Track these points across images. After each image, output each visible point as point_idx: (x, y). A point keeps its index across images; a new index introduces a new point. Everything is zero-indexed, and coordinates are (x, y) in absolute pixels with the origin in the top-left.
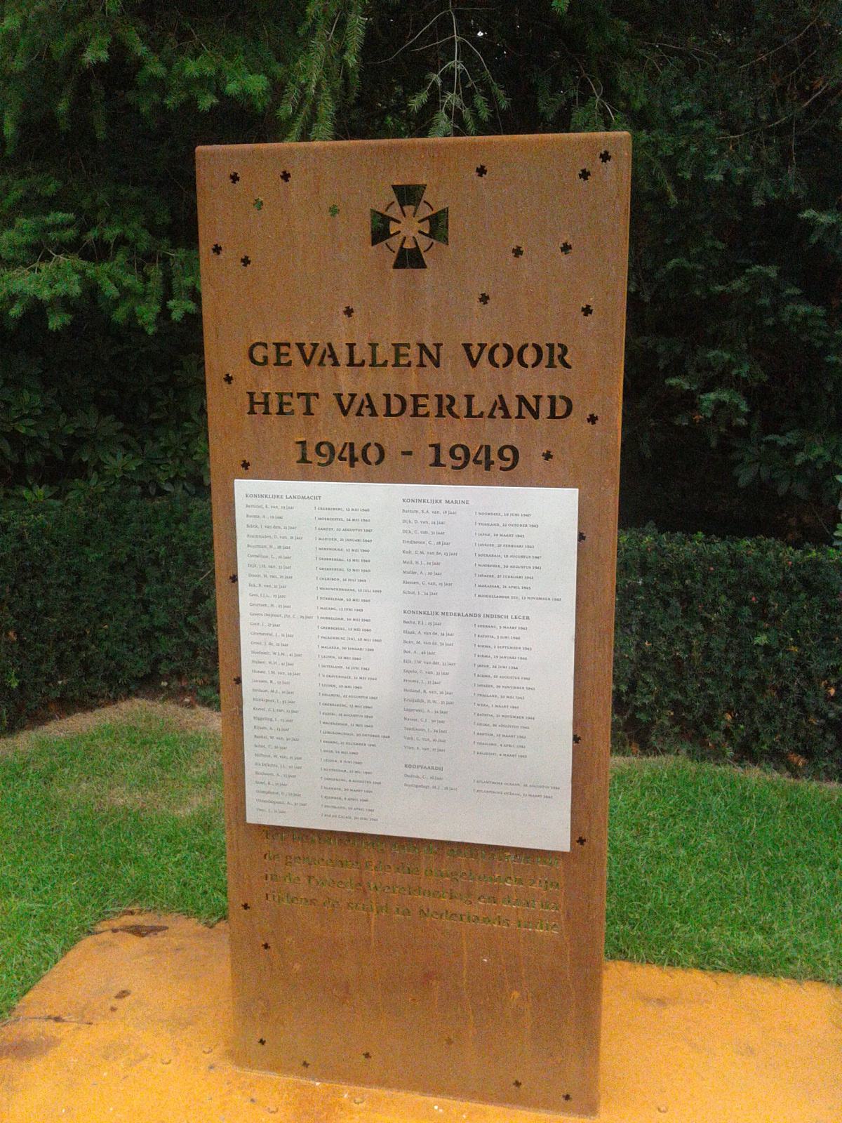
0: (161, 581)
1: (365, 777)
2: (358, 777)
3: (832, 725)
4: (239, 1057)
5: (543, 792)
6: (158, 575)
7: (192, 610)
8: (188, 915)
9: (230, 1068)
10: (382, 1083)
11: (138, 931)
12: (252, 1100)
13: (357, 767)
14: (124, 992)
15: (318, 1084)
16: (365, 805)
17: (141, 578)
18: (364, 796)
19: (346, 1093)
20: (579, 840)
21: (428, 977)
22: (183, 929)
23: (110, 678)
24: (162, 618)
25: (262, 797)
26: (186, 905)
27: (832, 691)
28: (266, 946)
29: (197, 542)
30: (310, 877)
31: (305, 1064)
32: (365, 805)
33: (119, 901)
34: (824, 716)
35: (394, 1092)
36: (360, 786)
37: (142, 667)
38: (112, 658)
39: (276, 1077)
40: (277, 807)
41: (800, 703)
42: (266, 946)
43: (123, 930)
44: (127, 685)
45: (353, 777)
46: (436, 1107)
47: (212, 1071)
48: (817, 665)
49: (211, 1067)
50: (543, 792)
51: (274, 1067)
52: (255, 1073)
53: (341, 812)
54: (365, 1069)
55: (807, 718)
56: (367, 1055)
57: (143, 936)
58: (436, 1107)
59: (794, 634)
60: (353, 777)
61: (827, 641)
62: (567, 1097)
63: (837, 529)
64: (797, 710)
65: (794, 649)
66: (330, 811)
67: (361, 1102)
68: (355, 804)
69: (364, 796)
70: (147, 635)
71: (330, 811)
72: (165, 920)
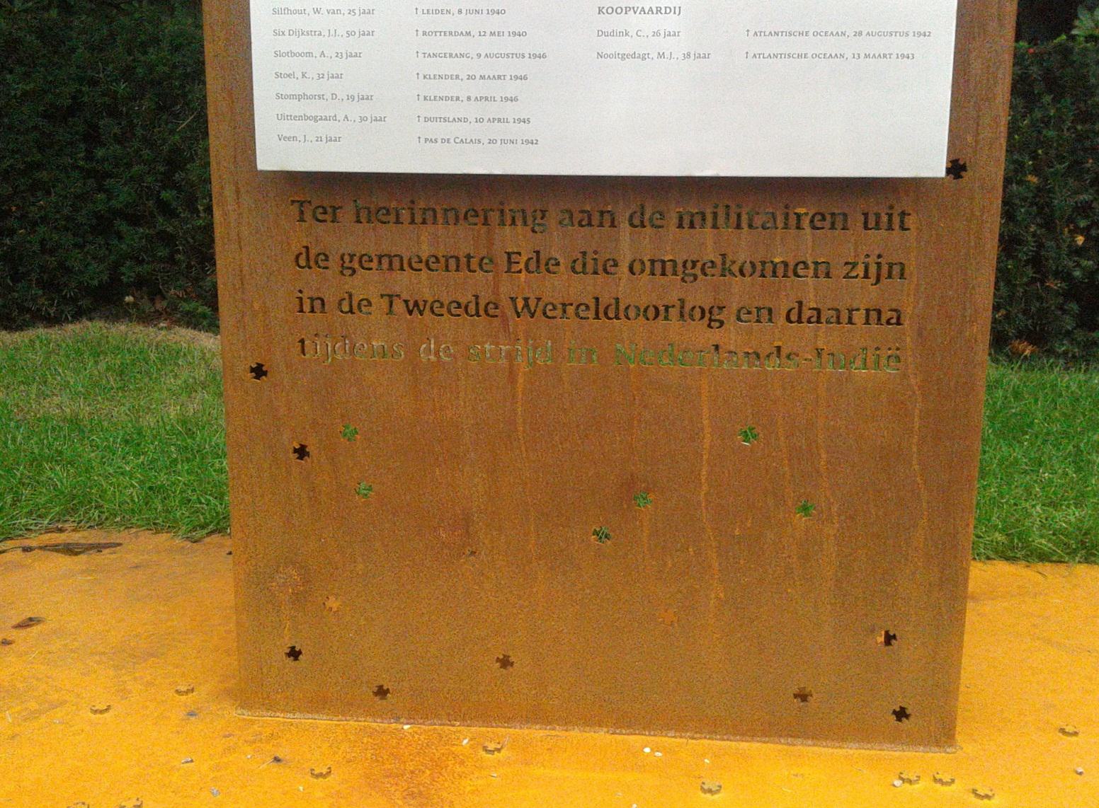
0: (119, 140)
1: (512, 45)
2: (497, 45)
3: (1073, 292)
4: (251, 691)
5: (899, 45)
6: (116, 130)
7: (167, 181)
8: (155, 527)
9: (233, 714)
10: (537, 715)
11: (70, 550)
12: (277, 760)
13: (495, 23)
14: (31, 619)
15: (406, 727)
16: (510, 111)
17: (92, 137)
18: (511, 88)
19: (465, 737)
20: (956, 168)
21: (630, 490)
22: (143, 546)
23: (51, 286)
24: (124, 195)
25: (292, 107)
26: (155, 511)
27: (1080, 240)
28: (302, 452)
29: (174, 67)
30: (391, 298)
31: (382, 692)
32: (510, 111)
33: (37, 513)
34: (1067, 277)
35: (559, 732)
36: (501, 66)
37: (96, 273)
38: (52, 252)
39: (323, 722)
40: (323, 128)
41: (1036, 261)
42: (302, 452)
43: (40, 548)
44: (74, 300)
45: (486, 45)
46: (647, 750)
47: (193, 719)
48: (1063, 200)
49: (191, 714)
50: (899, 45)
51: (319, 704)
52: (281, 718)
53: (461, 130)
54: (505, 691)
55: (1042, 282)
56: (505, 662)
57: (77, 554)
58: (647, 750)
59: (1034, 157)
60: (486, 45)
61: (1076, 168)
62: (901, 714)
63: (1076, 27)
64: (1030, 271)
65: (1033, 179)
66: (440, 130)
67: (499, 750)
68: (493, 110)
69: (511, 88)
70: (103, 225)
71: (440, 130)
72: (115, 537)
